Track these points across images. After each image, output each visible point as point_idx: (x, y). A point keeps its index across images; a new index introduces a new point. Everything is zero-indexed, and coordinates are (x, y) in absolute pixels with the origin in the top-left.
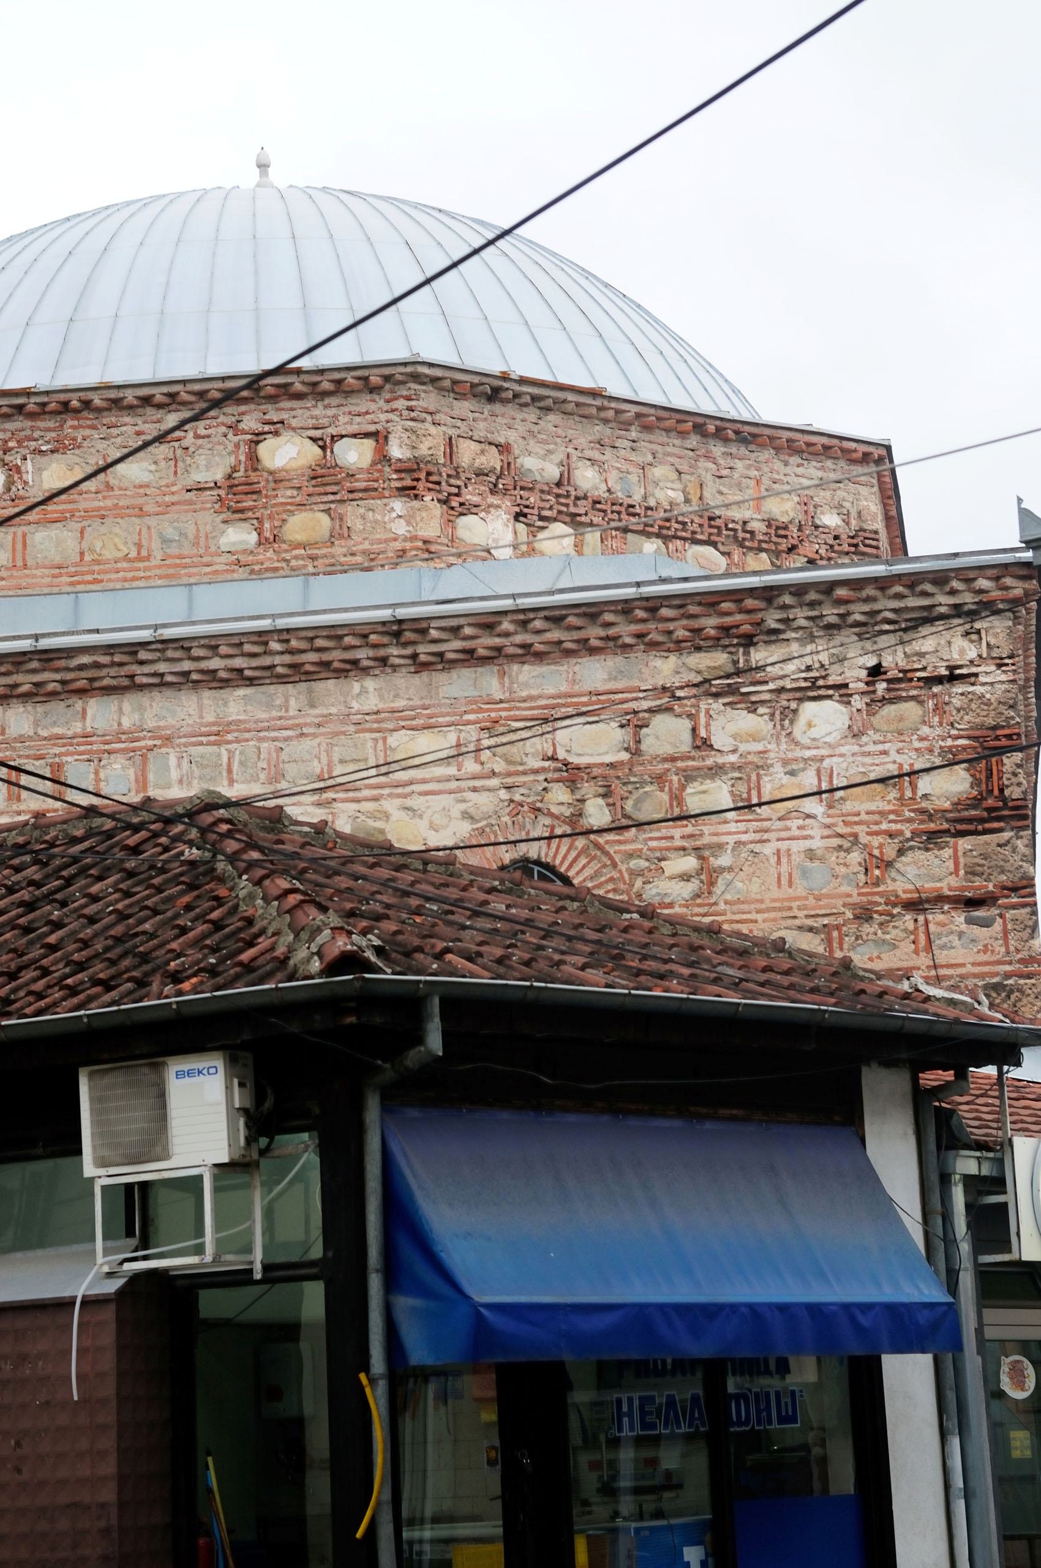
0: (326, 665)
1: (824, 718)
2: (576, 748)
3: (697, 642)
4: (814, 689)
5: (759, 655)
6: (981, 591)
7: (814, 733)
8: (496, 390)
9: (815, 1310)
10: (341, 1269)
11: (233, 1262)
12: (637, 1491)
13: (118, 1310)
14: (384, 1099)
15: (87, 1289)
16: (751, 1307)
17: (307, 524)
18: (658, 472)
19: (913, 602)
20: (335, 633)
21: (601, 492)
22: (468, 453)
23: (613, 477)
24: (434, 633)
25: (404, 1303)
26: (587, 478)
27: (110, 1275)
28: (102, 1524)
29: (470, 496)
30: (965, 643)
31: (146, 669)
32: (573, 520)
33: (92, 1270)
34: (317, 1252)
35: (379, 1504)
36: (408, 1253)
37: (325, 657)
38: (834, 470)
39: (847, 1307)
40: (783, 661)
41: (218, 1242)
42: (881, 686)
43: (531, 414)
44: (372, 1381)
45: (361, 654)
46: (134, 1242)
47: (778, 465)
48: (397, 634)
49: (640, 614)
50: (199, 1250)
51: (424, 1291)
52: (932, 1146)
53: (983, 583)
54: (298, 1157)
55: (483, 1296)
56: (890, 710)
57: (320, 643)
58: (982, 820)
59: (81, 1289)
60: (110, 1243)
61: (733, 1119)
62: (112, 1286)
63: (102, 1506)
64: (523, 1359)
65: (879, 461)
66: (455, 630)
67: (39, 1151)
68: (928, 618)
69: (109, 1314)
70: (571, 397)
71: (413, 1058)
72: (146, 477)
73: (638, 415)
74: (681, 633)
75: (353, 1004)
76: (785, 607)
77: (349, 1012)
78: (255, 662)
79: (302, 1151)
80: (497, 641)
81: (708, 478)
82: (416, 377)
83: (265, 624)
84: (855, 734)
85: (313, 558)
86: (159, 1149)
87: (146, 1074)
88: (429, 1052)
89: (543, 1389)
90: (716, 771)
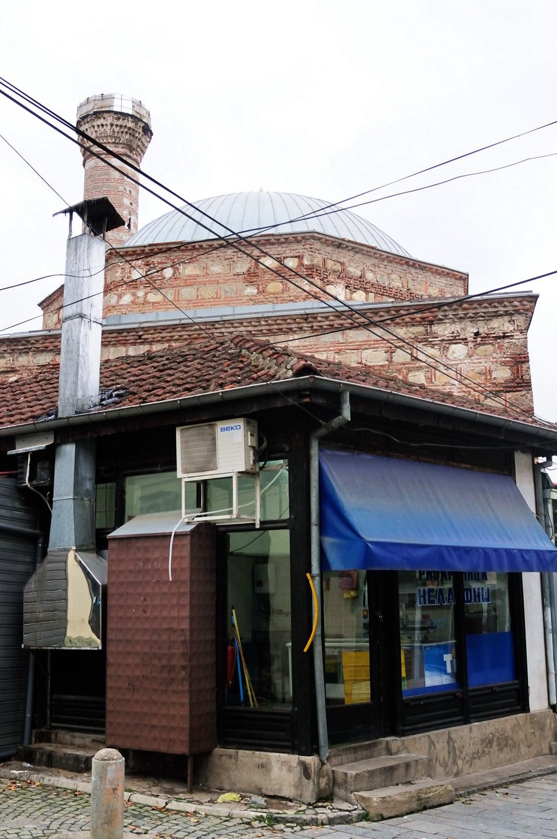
0: (281, 330)
1: (458, 351)
2: (369, 360)
3: (413, 323)
4: (455, 339)
5: (435, 328)
6: (515, 306)
7: (455, 355)
8: (340, 244)
9: (508, 552)
10: (298, 526)
11: (246, 519)
12: (414, 629)
13: (191, 539)
14: (319, 444)
15: (179, 528)
16: (483, 549)
17: (275, 286)
18: (393, 276)
19: (490, 310)
20: (284, 318)
21: (375, 281)
22: (330, 264)
23: (378, 277)
24: (319, 319)
25: (328, 540)
26: (370, 276)
27: (188, 523)
28: (183, 638)
29: (331, 279)
30: (509, 325)
31: (218, 331)
32: (365, 290)
33: (182, 520)
34: (286, 516)
35: (315, 636)
36: (331, 516)
37: (280, 327)
38: (450, 281)
39: (520, 551)
40: (443, 330)
41: (239, 510)
42: (479, 339)
43: (352, 253)
44: (312, 577)
45: (293, 326)
46: (201, 509)
47: (432, 278)
48: (306, 319)
49: (393, 312)
50: (230, 512)
51: (338, 534)
52: (541, 487)
53: (516, 303)
54: (277, 471)
55: (369, 539)
56: (482, 348)
57: (279, 322)
58: (515, 387)
59: (174, 529)
60: (189, 511)
61: (467, 469)
62: (189, 528)
63: (183, 630)
64: (387, 569)
65: (464, 280)
66: (327, 318)
67: (159, 469)
68: (496, 315)
69: (187, 541)
70: (365, 248)
71: (336, 422)
72: (220, 271)
73: (387, 257)
74: (407, 320)
75: (308, 393)
76: (445, 311)
77: (306, 396)
78: (256, 329)
79: (280, 468)
80: (342, 322)
81: (410, 280)
82: (313, 238)
83: (260, 315)
84: (470, 356)
85: (276, 298)
86: (212, 465)
87: (206, 429)
88: (344, 419)
89: (384, 584)
90: (419, 368)
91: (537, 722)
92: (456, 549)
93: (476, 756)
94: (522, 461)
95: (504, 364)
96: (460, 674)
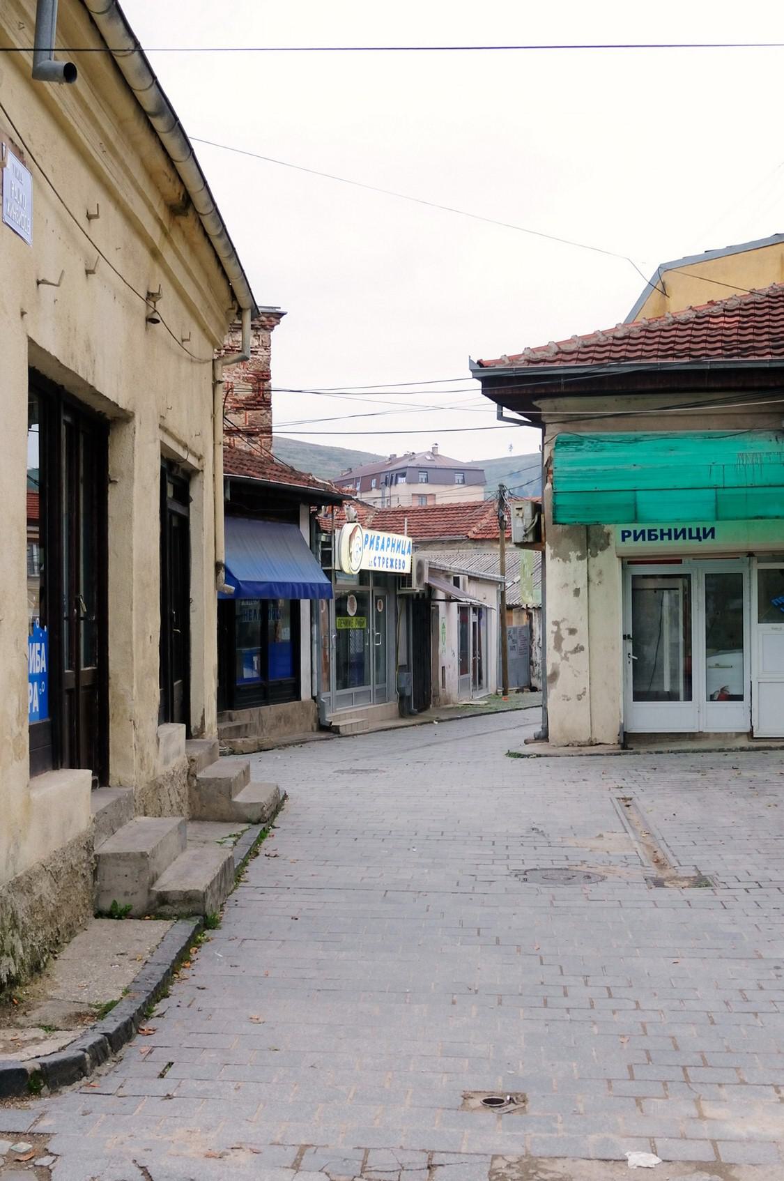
53: (263, 318)
91: (304, 707)
92: (279, 583)
93: (274, 727)
94: (304, 512)
95: (247, 380)
96: (264, 670)
